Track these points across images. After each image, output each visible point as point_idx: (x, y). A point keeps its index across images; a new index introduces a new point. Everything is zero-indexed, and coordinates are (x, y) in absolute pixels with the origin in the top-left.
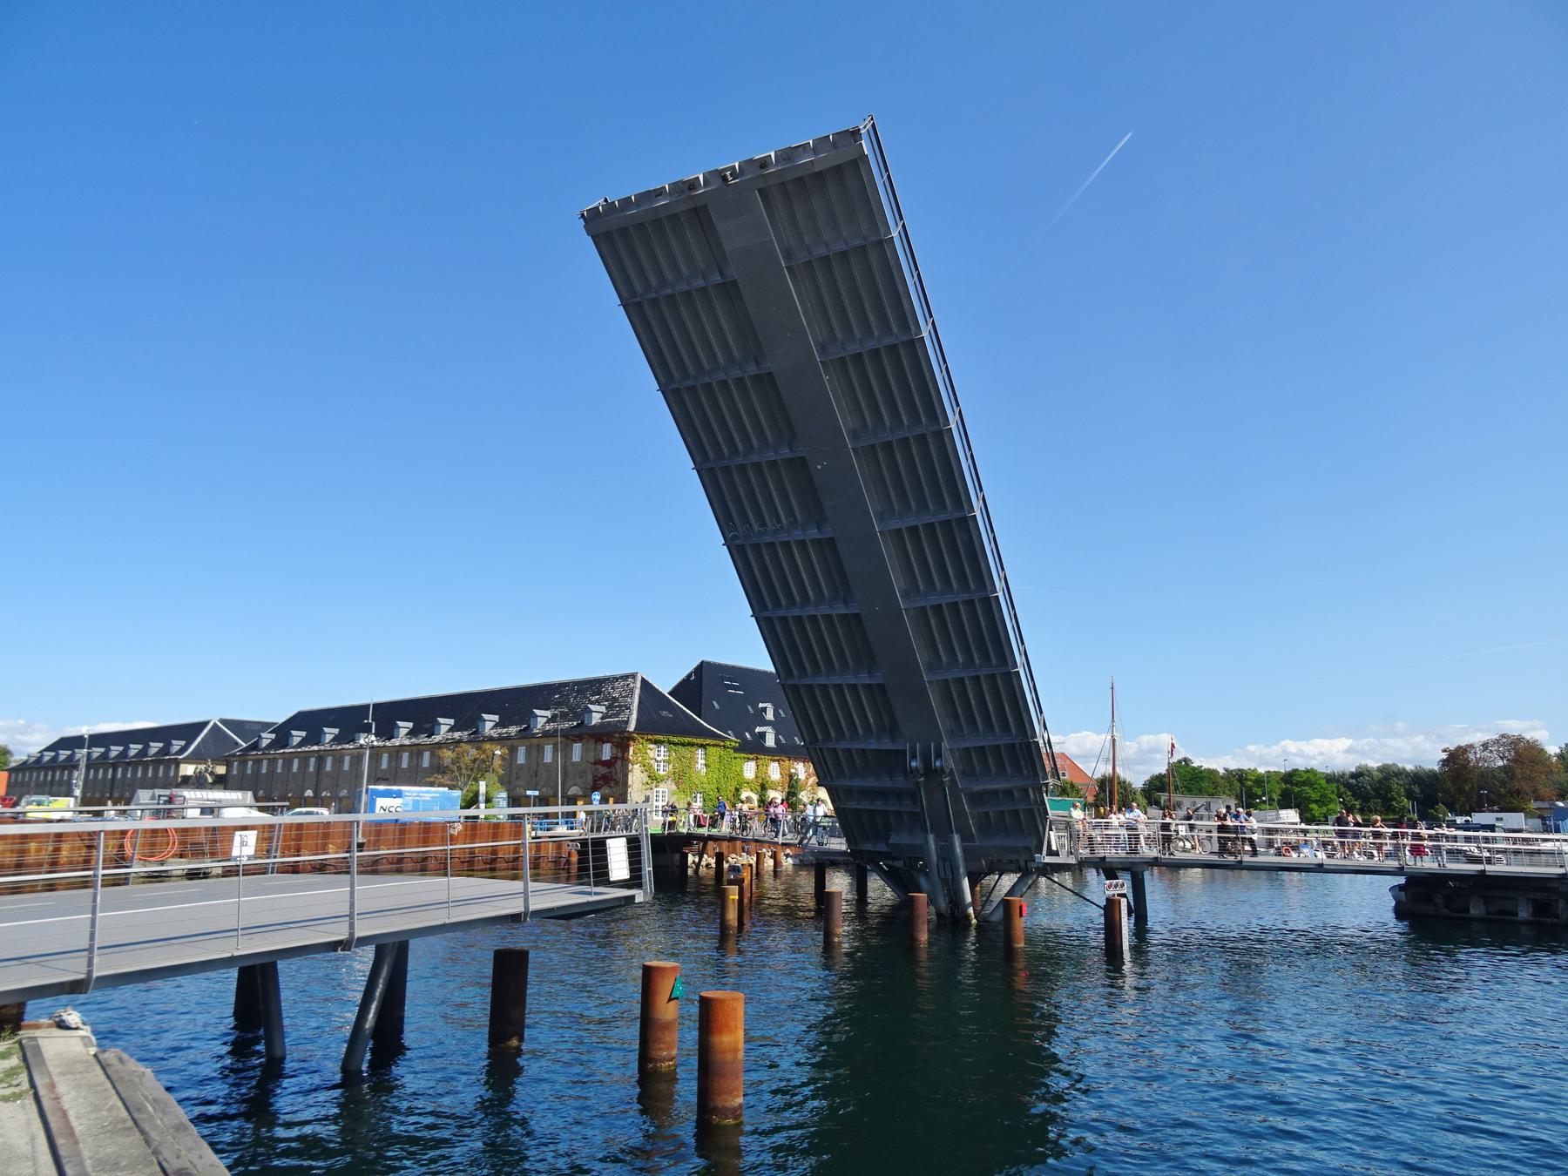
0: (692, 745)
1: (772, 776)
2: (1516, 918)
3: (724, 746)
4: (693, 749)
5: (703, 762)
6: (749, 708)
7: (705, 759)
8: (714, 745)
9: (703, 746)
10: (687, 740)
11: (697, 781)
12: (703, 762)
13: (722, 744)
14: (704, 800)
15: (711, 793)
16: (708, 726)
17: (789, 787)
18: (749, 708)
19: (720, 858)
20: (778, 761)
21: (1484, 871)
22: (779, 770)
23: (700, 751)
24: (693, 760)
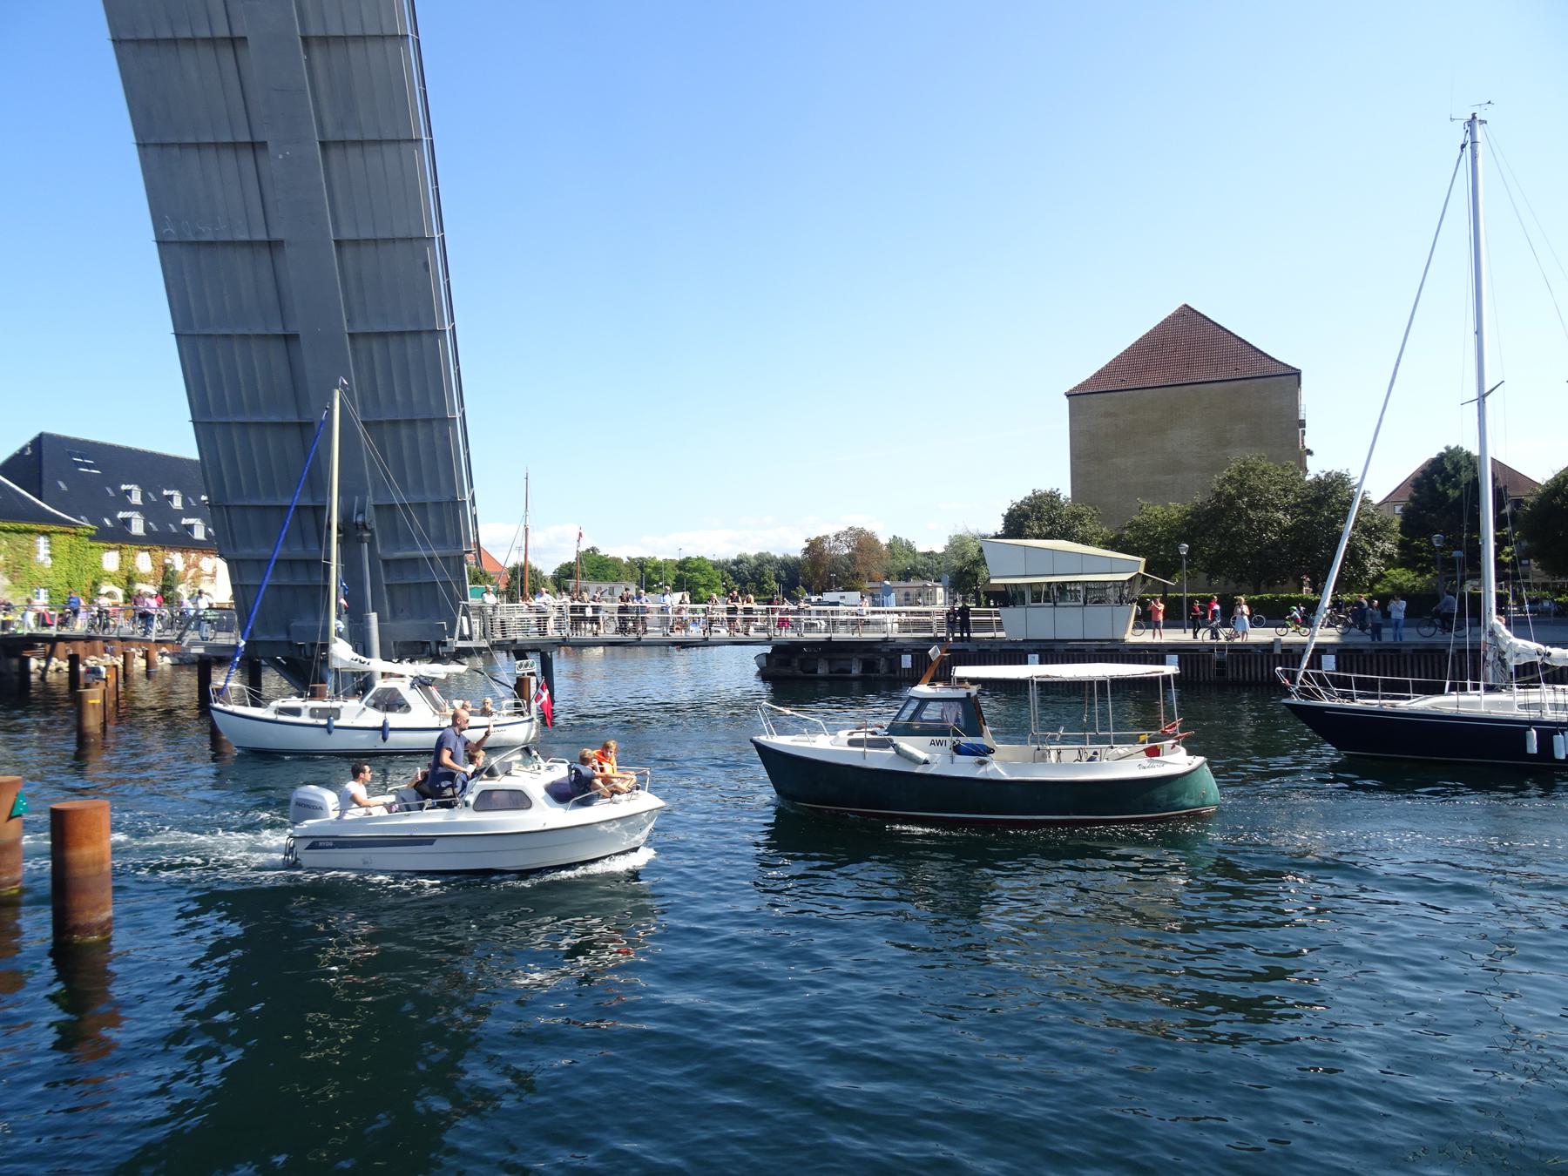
0: (31, 532)
3: (75, 534)
4: (32, 537)
6: (109, 490)
7: (50, 549)
8: (61, 533)
10: (23, 526)
11: (39, 575)
13: (73, 531)
14: (51, 597)
15: (60, 588)
16: (53, 510)
18: (109, 490)
19: (74, 660)
20: (149, 550)
21: (830, 638)
23: (42, 540)
24: (32, 550)
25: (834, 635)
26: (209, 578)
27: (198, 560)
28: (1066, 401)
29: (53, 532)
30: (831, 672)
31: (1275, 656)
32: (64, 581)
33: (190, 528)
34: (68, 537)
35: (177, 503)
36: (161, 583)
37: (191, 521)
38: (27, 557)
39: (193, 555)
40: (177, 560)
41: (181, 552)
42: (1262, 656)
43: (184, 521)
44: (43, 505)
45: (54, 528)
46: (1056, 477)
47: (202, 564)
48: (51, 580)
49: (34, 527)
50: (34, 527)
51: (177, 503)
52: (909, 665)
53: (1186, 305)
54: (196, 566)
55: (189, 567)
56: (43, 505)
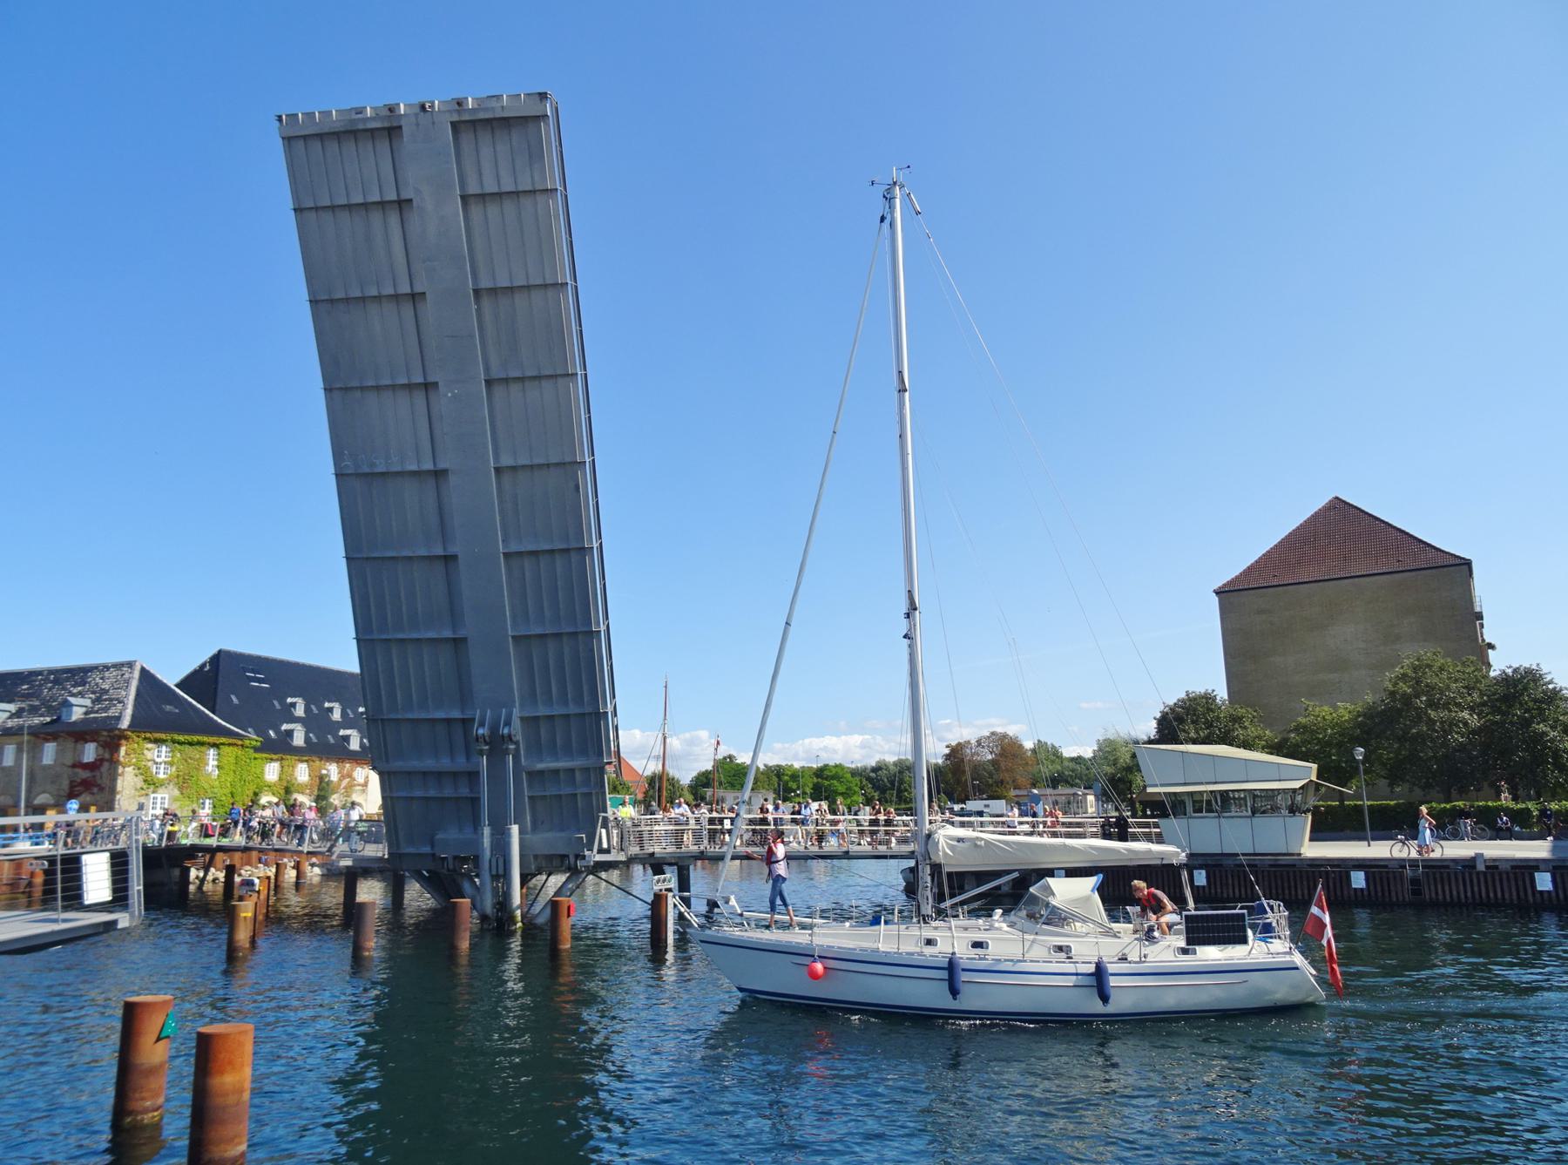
0: (201, 744)
1: (299, 778)
3: (242, 746)
5: (216, 763)
6: (276, 703)
7: (218, 760)
8: (229, 745)
9: (215, 745)
10: (195, 738)
11: (206, 786)
12: (216, 763)
13: (240, 743)
14: (214, 807)
15: (224, 798)
16: (224, 723)
17: (319, 789)
18: (276, 703)
19: (231, 871)
20: (307, 761)
23: (212, 752)
26: (360, 788)
27: (352, 770)
28: (1216, 599)
31: (1478, 873)
32: (227, 791)
34: (235, 749)
35: (337, 715)
36: (316, 793)
37: (348, 732)
39: (348, 765)
40: (332, 771)
41: (337, 762)
42: (1463, 873)
43: (342, 732)
44: (216, 718)
45: (223, 740)
46: (1212, 679)
47: (355, 774)
48: (216, 790)
49: (205, 739)
50: (205, 739)
53: (1337, 498)
54: (349, 776)
56: (216, 718)
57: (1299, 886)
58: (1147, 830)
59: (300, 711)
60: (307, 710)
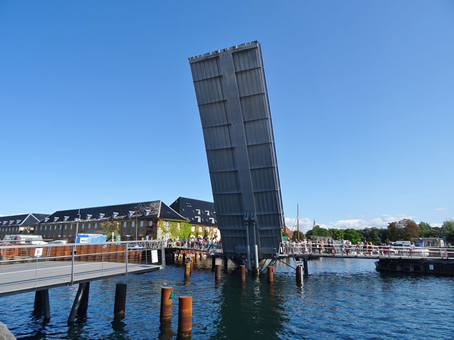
0: (176, 221)
2: (409, 271)
3: (186, 222)
4: (177, 223)
5: (180, 226)
7: (180, 226)
8: (183, 222)
9: (180, 222)
10: (175, 220)
12: (180, 226)
13: (185, 221)
14: (180, 238)
15: (182, 236)
19: (184, 255)
20: (202, 226)
21: (401, 258)
22: (202, 229)
23: (179, 223)
24: (176, 226)
25: (402, 257)
29: (181, 222)
30: (402, 270)
32: (183, 234)
33: (211, 220)
35: (208, 214)
36: (204, 235)
37: (211, 218)
38: (175, 228)
39: (212, 227)
40: (208, 229)
45: (181, 221)
47: (213, 230)
51: (208, 214)
52: (433, 269)
55: (210, 231)
57: (441, 270)
58: (438, 252)
59: (199, 213)
60: (201, 213)
